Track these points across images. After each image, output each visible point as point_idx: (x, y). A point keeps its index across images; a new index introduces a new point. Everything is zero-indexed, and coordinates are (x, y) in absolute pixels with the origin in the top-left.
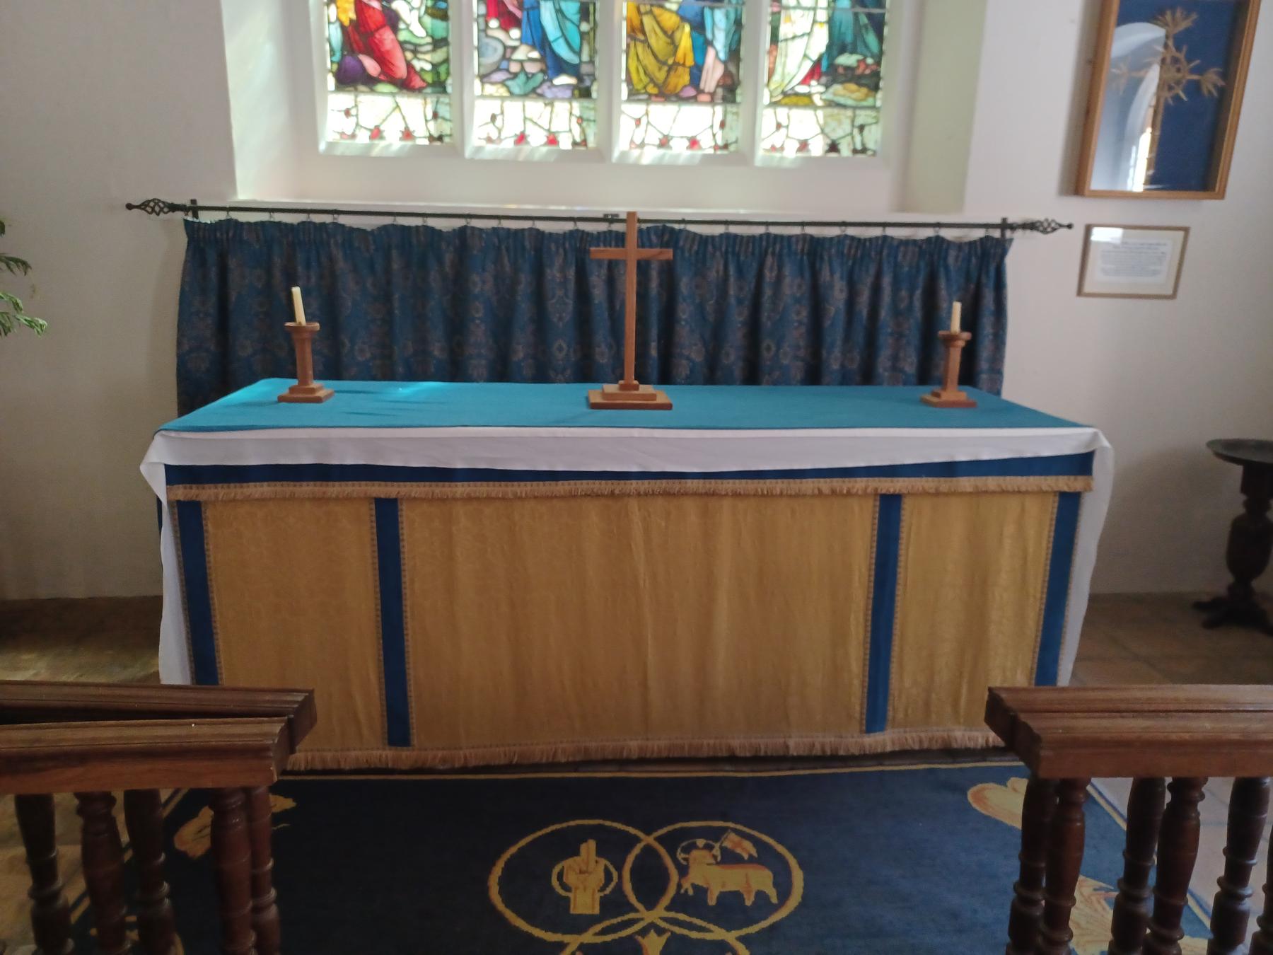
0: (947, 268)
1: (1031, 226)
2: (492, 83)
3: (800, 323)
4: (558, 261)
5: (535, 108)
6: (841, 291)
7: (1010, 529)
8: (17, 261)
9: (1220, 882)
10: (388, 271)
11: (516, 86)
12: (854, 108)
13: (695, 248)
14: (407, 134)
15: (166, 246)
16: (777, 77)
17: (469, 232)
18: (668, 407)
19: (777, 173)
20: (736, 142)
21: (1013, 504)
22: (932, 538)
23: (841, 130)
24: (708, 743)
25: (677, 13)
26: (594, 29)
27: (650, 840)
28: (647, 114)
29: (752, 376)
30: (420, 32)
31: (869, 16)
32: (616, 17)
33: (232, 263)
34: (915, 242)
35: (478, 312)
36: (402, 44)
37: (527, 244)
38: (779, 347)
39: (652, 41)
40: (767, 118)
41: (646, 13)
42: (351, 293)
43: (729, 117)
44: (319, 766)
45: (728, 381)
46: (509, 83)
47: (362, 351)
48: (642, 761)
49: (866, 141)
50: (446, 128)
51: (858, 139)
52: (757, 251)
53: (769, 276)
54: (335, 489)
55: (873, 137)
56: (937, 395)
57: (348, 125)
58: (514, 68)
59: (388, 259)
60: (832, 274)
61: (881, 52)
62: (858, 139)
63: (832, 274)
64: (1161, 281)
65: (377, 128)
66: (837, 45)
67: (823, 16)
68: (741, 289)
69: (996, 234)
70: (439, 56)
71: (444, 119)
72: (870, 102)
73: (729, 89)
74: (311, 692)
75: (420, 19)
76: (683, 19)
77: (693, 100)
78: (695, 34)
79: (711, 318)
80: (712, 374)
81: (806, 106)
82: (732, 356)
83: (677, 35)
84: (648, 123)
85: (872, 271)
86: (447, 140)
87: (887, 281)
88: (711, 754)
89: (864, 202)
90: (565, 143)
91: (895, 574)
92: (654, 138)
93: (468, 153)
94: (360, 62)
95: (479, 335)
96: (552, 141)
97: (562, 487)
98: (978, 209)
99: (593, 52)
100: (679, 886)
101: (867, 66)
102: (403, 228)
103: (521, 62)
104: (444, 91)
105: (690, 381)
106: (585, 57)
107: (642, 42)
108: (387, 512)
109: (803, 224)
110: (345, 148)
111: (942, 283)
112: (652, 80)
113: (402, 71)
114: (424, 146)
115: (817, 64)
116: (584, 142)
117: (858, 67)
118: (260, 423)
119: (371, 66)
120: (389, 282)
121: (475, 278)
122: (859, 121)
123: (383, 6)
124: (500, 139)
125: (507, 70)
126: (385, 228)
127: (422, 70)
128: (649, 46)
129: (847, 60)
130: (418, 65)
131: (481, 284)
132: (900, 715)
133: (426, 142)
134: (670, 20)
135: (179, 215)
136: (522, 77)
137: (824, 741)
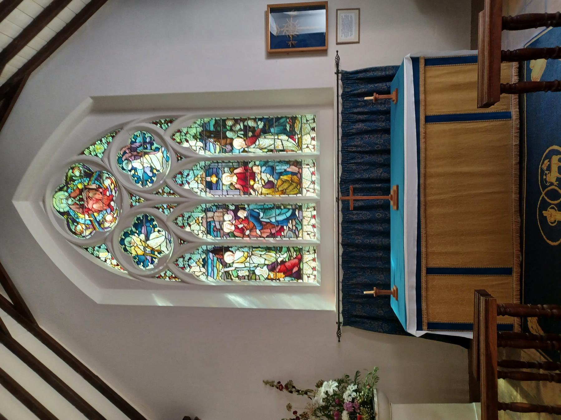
0: (351, 91)
1: (337, 65)
3: (369, 137)
4: (351, 216)
5: (305, 222)
7: (437, 80)
8: (356, 374)
9: (508, 84)
10: (356, 268)
11: (299, 228)
12: (302, 123)
14: (314, 260)
15: (349, 332)
16: (294, 149)
18: (398, 187)
19: (321, 148)
21: (429, 81)
22: (439, 104)
24: (515, 171)
27: (543, 193)
29: (388, 152)
30: (285, 255)
32: (280, 198)
33: (355, 313)
34: (343, 103)
35: (367, 241)
38: (377, 144)
39: (285, 187)
40: (306, 151)
42: (362, 279)
44: (519, 297)
45: (389, 160)
47: (381, 277)
48: (520, 193)
50: (312, 248)
53: (354, 149)
54: (423, 285)
55: (310, 117)
56: (394, 101)
57: (312, 277)
58: (294, 228)
59: (352, 267)
62: (310, 121)
64: (353, 15)
66: (284, 132)
67: (276, 137)
68: (358, 158)
69: (340, 75)
70: (292, 250)
73: (298, 164)
74: (475, 290)
79: (368, 167)
80: (387, 165)
82: (380, 159)
85: (352, 115)
87: (355, 110)
88: (518, 170)
89: (330, 118)
90: (315, 213)
91: (452, 115)
92: (312, 186)
93: (318, 242)
95: (374, 241)
96: (314, 217)
97: (423, 220)
98: (331, 81)
99: (289, 205)
100: (556, 186)
102: (342, 262)
105: (389, 172)
106: (290, 207)
108: (431, 271)
110: (319, 278)
111: (356, 92)
115: (289, 137)
116: (314, 207)
118: (405, 307)
119: (295, 269)
120: (359, 268)
121: (357, 242)
122: (305, 122)
124: (314, 232)
126: (342, 268)
131: (359, 240)
132: (505, 107)
133: (316, 254)
135: (341, 327)
137: (514, 133)
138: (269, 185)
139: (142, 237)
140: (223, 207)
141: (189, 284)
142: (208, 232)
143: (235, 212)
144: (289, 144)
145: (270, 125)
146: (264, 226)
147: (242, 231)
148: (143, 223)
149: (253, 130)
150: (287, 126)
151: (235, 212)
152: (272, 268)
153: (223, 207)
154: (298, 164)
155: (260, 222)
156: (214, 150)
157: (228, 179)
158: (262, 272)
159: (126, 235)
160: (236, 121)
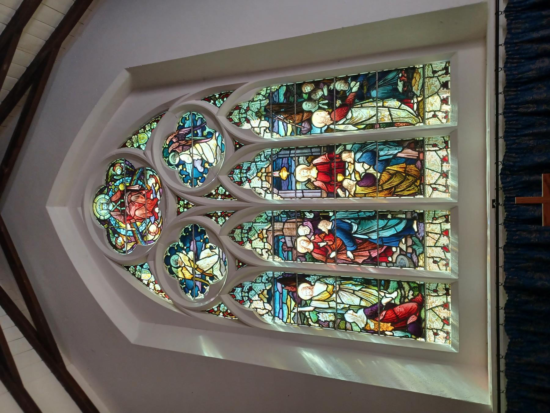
2: (418, 262)
4: (524, 234)
5: (429, 242)
6: (543, 62)
12: (424, 78)
13: (514, 155)
17: (507, 285)
20: (443, 137)
23: (436, 83)
25: (381, 173)
26: (390, 212)
28: (430, 185)
30: (395, 295)
31: (379, 80)
36: (401, 303)
37: (514, 252)
39: (395, 184)
40: (432, 122)
41: (382, 188)
43: (431, 142)
46: (418, 254)
49: (441, 69)
50: (441, 287)
51: (440, 73)
52: (516, 118)
53: (532, 108)
55: (439, 65)
58: (410, 250)
60: (531, 70)
61: (396, 70)
62: (440, 73)
63: (531, 70)
65: (442, 321)
66: (394, 94)
71: (437, 287)
72: (420, 71)
73: (418, 145)
75: (389, 293)
76: (384, 170)
77: (423, 162)
78: (391, 164)
81: (424, 104)
83: (391, 172)
84: (434, 184)
85: (529, 46)
86: (448, 287)
87: (535, 35)
92: (442, 181)
93: (454, 277)
94: (410, 323)
96: (445, 233)
101: (402, 76)
103: (407, 247)
104: (424, 285)
106: (404, 216)
107: (395, 189)
109: (497, 94)
112: (413, 183)
113: (414, 305)
114: (451, 298)
116: (446, 216)
117: (403, 80)
119: (412, 319)
123: (385, 310)
124: (446, 259)
125: (411, 254)
127: (413, 295)
128: (397, 185)
129: (400, 88)
130: (411, 297)
134: (385, 176)
136: (414, 247)
138: (367, 180)
139: (191, 254)
140: (296, 215)
141: (248, 327)
142: (276, 252)
143: (315, 222)
144: (402, 112)
145: (371, 85)
146: (359, 245)
147: (325, 252)
148: (193, 236)
149: (342, 95)
150: (401, 85)
151: (315, 222)
152: (373, 313)
153: (296, 215)
154: (418, 145)
155: (353, 240)
156: (284, 131)
157: (304, 173)
158: (358, 319)
159: (173, 251)
160: (317, 85)
